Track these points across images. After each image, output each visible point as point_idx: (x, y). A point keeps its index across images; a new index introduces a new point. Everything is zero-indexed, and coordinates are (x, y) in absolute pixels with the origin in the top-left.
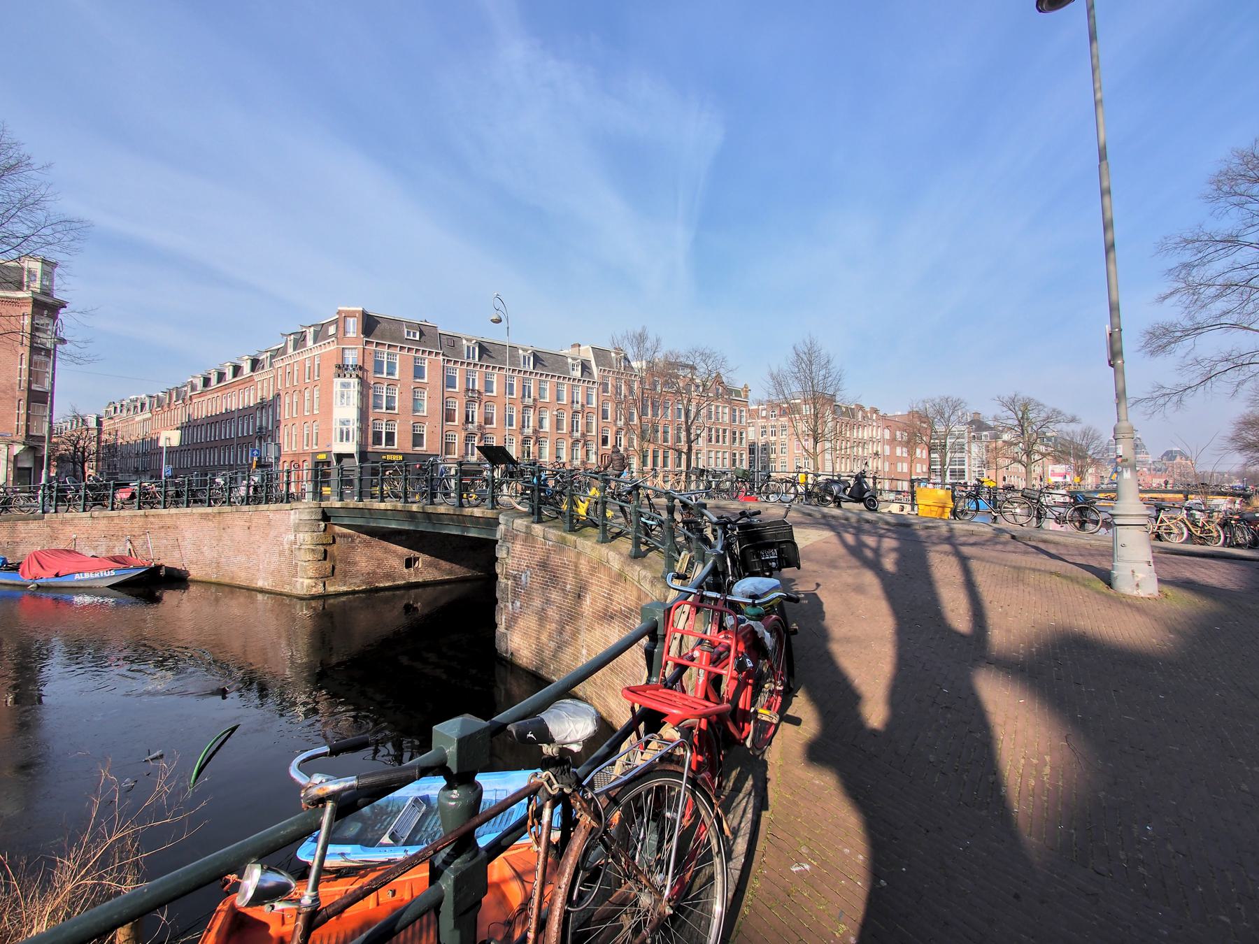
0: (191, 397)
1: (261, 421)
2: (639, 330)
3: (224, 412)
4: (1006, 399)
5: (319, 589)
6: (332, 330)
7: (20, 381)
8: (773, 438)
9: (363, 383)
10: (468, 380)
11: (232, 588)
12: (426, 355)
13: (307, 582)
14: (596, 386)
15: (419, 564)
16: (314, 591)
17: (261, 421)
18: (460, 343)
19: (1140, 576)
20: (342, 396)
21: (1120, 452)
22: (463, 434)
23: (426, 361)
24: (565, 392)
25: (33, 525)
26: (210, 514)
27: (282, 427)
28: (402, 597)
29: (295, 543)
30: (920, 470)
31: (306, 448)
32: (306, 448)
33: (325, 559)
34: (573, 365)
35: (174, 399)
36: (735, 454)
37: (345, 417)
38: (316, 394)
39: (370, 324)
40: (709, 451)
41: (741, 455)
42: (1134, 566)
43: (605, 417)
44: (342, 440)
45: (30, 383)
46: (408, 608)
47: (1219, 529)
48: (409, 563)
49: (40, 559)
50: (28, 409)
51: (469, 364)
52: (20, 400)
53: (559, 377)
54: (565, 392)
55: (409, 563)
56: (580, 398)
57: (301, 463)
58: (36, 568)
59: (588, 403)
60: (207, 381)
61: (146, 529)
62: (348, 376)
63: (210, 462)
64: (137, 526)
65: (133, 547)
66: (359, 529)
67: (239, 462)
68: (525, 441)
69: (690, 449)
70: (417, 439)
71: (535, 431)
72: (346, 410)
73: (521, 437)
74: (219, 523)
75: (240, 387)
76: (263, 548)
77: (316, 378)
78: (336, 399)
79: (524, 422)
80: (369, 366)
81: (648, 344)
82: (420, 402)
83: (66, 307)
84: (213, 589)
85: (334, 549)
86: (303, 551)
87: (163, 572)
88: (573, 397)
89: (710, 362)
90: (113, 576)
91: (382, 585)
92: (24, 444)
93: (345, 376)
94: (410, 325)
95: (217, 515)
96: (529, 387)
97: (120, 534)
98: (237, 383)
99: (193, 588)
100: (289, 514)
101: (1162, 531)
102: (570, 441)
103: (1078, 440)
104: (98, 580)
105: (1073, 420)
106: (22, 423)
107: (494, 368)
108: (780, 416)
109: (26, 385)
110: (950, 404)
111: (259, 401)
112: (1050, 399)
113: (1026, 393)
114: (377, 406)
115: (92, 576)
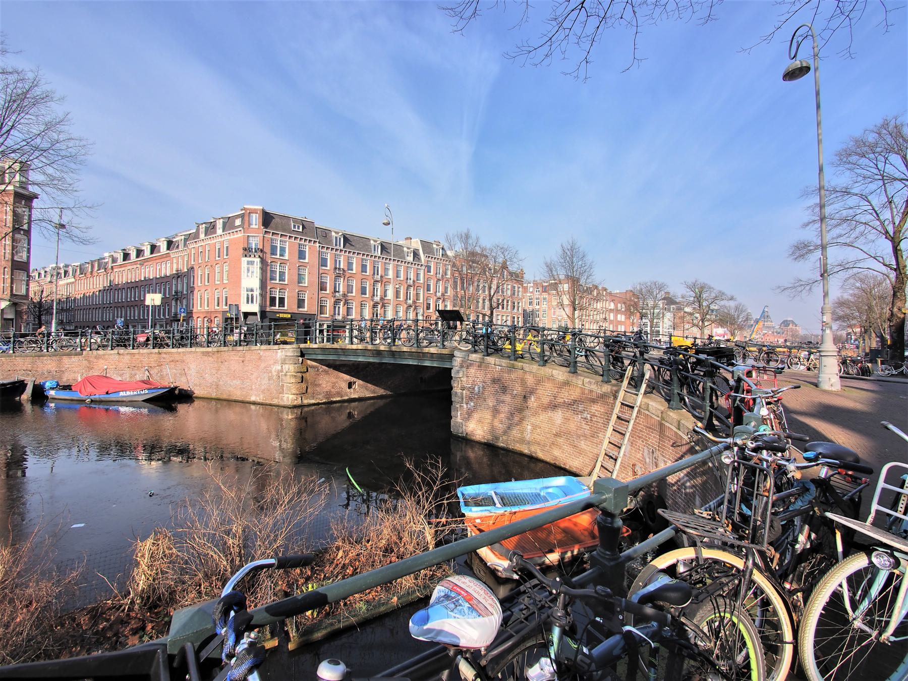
0: (112, 267)
1: (177, 287)
2: (466, 231)
3: (143, 279)
4: (690, 283)
5: (299, 402)
6: (238, 222)
7: (5, 253)
8: (538, 307)
9: (263, 261)
10: (336, 261)
11: (230, 402)
12: (307, 243)
13: (291, 397)
14: (423, 267)
15: (356, 386)
16: (295, 403)
17: (177, 287)
18: (330, 235)
19: (833, 381)
20: (248, 270)
21: (825, 320)
22: (333, 300)
23: (307, 247)
24: (402, 272)
25: (75, 359)
26: (210, 352)
27: (196, 292)
28: (346, 408)
29: (282, 371)
31: (216, 308)
32: (216, 308)
33: (302, 382)
34: (408, 252)
35: (96, 268)
36: (514, 318)
37: (250, 286)
38: (226, 268)
39: (267, 219)
40: (498, 315)
41: (518, 318)
42: (830, 376)
43: (429, 290)
44: (248, 302)
45: (13, 255)
46: (350, 415)
47: (841, 365)
48: (350, 385)
49: (90, 381)
50: (12, 275)
51: (337, 250)
52: (5, 268)
53: (363, 254)
54: (402, 272)
55: (350, 385)
56: (412, 276)
57: (213, 319)
58: (90, 389)
59: (417, 280)
60: (126, 256)
61: (160, 362)
62: (253, 256)
63: (130, 317)
64: (152, 360)
65: (150, 374)
66: (321, 362)
67: (157, 317)
68: (375, 306)
69: (492, 313)
70: (301, 303)
71: (382, 299)
72: (251, 280)
73: (372, 303)
74: (218, 358)
75: (157, 261)
76: (255, 374)
77: (225, 257)
78: (244, 275)
79: (374, 293)
80: (268, 249)
81: (470, 241)
82: (303, 276)
83: (37, 198)
84: (214, 403)
85: (307, 376)
86: (288, 376)
87: (177, 392)
88: (407, 275)
89: (506, 254)
90: (147, 394)
91: (334, 399)
92: (10, 301)
93: (250, 256)
94: (296, 220)
95: (216, 353)
96: (378, 267)
97: (140, 365)
98: (154, 258)
99: (196, 403)
100: (277, 352)
101: (811, 366)
102: (405, 306)
103: (732, 312)
104: (137, 397)
105: (732, 299)
106: (8, 285)
107: (354, 253)
108: (543, 292)
109: (10, 257)
110: (657, 286)
111: (174, 272)
112: (717, 285)
113: (702, 280)
114: (272, 279)
115: (132, 393)
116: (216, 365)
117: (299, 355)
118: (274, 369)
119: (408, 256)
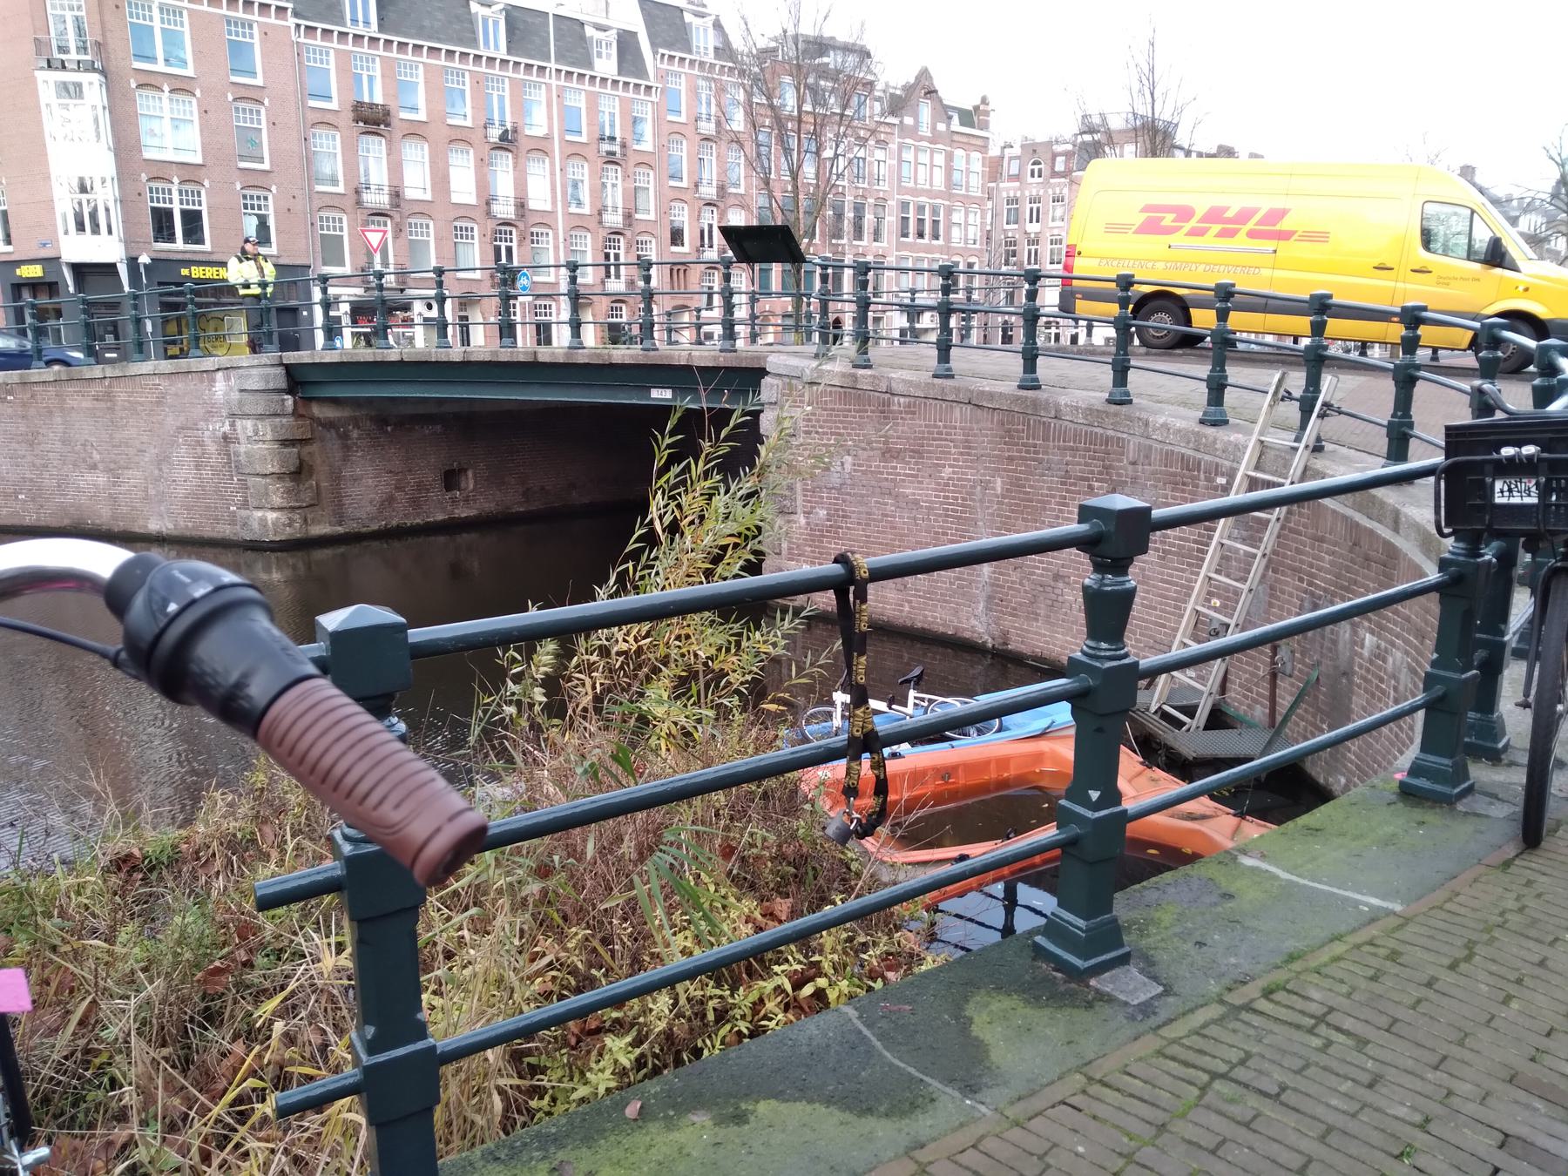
15: (469, 482)
30: (688, 1013)
55: (450, 480)
100: (214, 380)
116: (23, 429)
117: (284, 385)
118: (207, 433)
119: (599, 55)
